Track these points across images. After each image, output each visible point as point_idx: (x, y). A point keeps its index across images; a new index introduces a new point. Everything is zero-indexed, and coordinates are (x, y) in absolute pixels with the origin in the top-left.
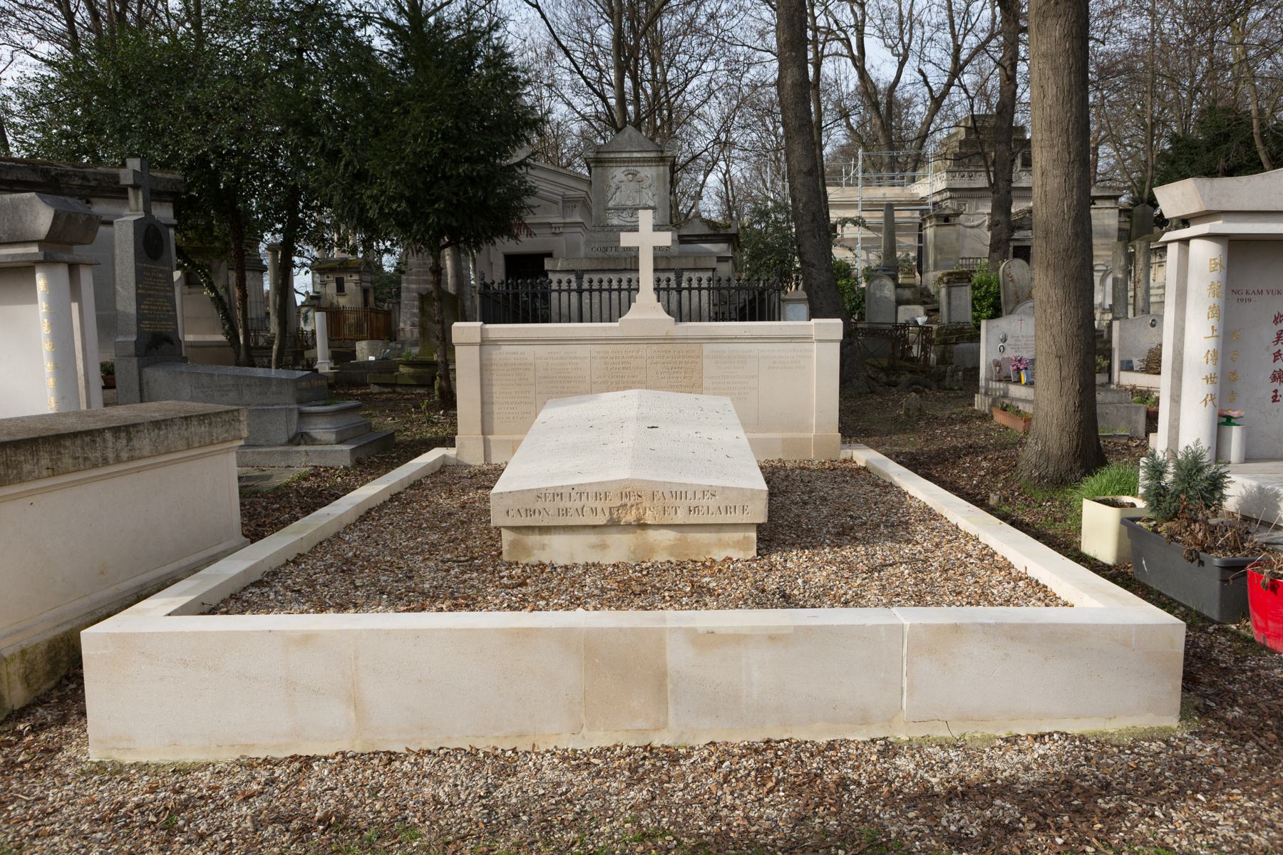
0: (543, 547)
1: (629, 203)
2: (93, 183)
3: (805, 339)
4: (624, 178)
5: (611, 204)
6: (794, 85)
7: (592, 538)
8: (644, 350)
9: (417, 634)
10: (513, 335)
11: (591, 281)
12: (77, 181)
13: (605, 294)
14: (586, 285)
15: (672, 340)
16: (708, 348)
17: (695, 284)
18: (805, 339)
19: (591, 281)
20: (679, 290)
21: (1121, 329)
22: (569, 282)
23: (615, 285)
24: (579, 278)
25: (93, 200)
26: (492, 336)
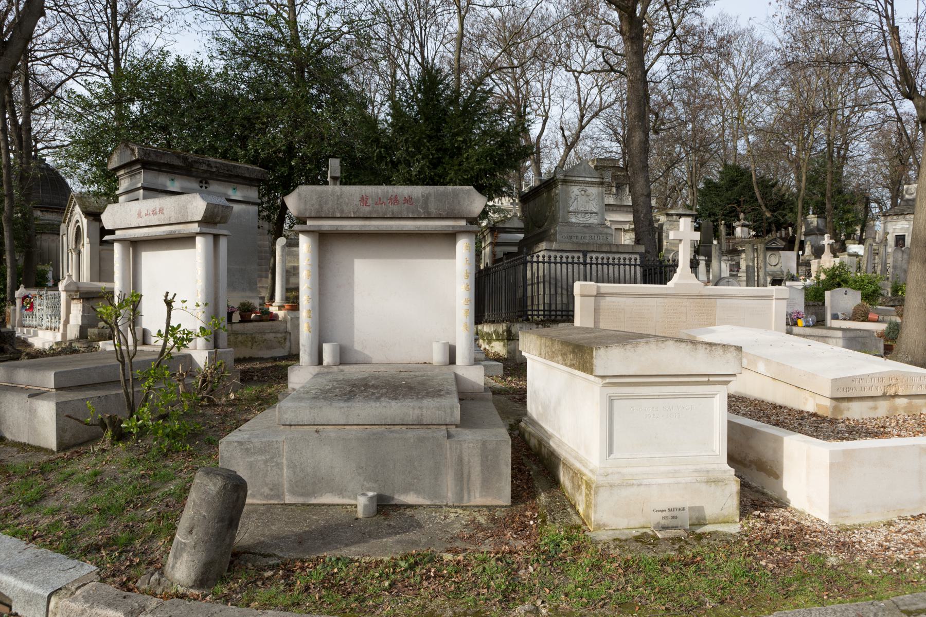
0: (848, 409)
1: (582, 209)
2: (214, 170)
3: (769, 298)
4: (579, 193)
5: (571, 209)
6: (640, 142)
7: (870, 404)
8: (686, 303)
9: (883, 449)
10: (614, 291)
11: (591, 258)
12: (204, 167)
13: (541, 265)
14: (588, 261)
15: (701, 296)
16: (720, 302)
17: (594, 261)
18: (769, 298)
19: (591, 258)
20: (585, 264)
21: (832, 296)
22: (579, 258)
23: (558, 260)
24: (585, 256)
25: (210, 181)
26: (602, 291)
